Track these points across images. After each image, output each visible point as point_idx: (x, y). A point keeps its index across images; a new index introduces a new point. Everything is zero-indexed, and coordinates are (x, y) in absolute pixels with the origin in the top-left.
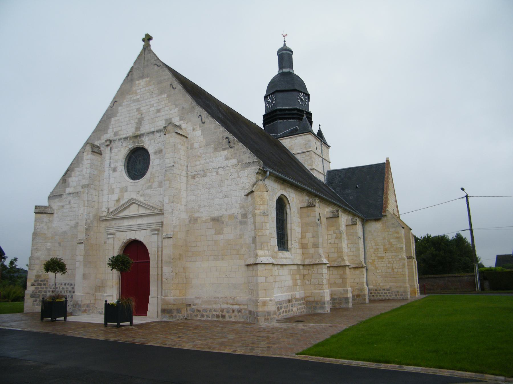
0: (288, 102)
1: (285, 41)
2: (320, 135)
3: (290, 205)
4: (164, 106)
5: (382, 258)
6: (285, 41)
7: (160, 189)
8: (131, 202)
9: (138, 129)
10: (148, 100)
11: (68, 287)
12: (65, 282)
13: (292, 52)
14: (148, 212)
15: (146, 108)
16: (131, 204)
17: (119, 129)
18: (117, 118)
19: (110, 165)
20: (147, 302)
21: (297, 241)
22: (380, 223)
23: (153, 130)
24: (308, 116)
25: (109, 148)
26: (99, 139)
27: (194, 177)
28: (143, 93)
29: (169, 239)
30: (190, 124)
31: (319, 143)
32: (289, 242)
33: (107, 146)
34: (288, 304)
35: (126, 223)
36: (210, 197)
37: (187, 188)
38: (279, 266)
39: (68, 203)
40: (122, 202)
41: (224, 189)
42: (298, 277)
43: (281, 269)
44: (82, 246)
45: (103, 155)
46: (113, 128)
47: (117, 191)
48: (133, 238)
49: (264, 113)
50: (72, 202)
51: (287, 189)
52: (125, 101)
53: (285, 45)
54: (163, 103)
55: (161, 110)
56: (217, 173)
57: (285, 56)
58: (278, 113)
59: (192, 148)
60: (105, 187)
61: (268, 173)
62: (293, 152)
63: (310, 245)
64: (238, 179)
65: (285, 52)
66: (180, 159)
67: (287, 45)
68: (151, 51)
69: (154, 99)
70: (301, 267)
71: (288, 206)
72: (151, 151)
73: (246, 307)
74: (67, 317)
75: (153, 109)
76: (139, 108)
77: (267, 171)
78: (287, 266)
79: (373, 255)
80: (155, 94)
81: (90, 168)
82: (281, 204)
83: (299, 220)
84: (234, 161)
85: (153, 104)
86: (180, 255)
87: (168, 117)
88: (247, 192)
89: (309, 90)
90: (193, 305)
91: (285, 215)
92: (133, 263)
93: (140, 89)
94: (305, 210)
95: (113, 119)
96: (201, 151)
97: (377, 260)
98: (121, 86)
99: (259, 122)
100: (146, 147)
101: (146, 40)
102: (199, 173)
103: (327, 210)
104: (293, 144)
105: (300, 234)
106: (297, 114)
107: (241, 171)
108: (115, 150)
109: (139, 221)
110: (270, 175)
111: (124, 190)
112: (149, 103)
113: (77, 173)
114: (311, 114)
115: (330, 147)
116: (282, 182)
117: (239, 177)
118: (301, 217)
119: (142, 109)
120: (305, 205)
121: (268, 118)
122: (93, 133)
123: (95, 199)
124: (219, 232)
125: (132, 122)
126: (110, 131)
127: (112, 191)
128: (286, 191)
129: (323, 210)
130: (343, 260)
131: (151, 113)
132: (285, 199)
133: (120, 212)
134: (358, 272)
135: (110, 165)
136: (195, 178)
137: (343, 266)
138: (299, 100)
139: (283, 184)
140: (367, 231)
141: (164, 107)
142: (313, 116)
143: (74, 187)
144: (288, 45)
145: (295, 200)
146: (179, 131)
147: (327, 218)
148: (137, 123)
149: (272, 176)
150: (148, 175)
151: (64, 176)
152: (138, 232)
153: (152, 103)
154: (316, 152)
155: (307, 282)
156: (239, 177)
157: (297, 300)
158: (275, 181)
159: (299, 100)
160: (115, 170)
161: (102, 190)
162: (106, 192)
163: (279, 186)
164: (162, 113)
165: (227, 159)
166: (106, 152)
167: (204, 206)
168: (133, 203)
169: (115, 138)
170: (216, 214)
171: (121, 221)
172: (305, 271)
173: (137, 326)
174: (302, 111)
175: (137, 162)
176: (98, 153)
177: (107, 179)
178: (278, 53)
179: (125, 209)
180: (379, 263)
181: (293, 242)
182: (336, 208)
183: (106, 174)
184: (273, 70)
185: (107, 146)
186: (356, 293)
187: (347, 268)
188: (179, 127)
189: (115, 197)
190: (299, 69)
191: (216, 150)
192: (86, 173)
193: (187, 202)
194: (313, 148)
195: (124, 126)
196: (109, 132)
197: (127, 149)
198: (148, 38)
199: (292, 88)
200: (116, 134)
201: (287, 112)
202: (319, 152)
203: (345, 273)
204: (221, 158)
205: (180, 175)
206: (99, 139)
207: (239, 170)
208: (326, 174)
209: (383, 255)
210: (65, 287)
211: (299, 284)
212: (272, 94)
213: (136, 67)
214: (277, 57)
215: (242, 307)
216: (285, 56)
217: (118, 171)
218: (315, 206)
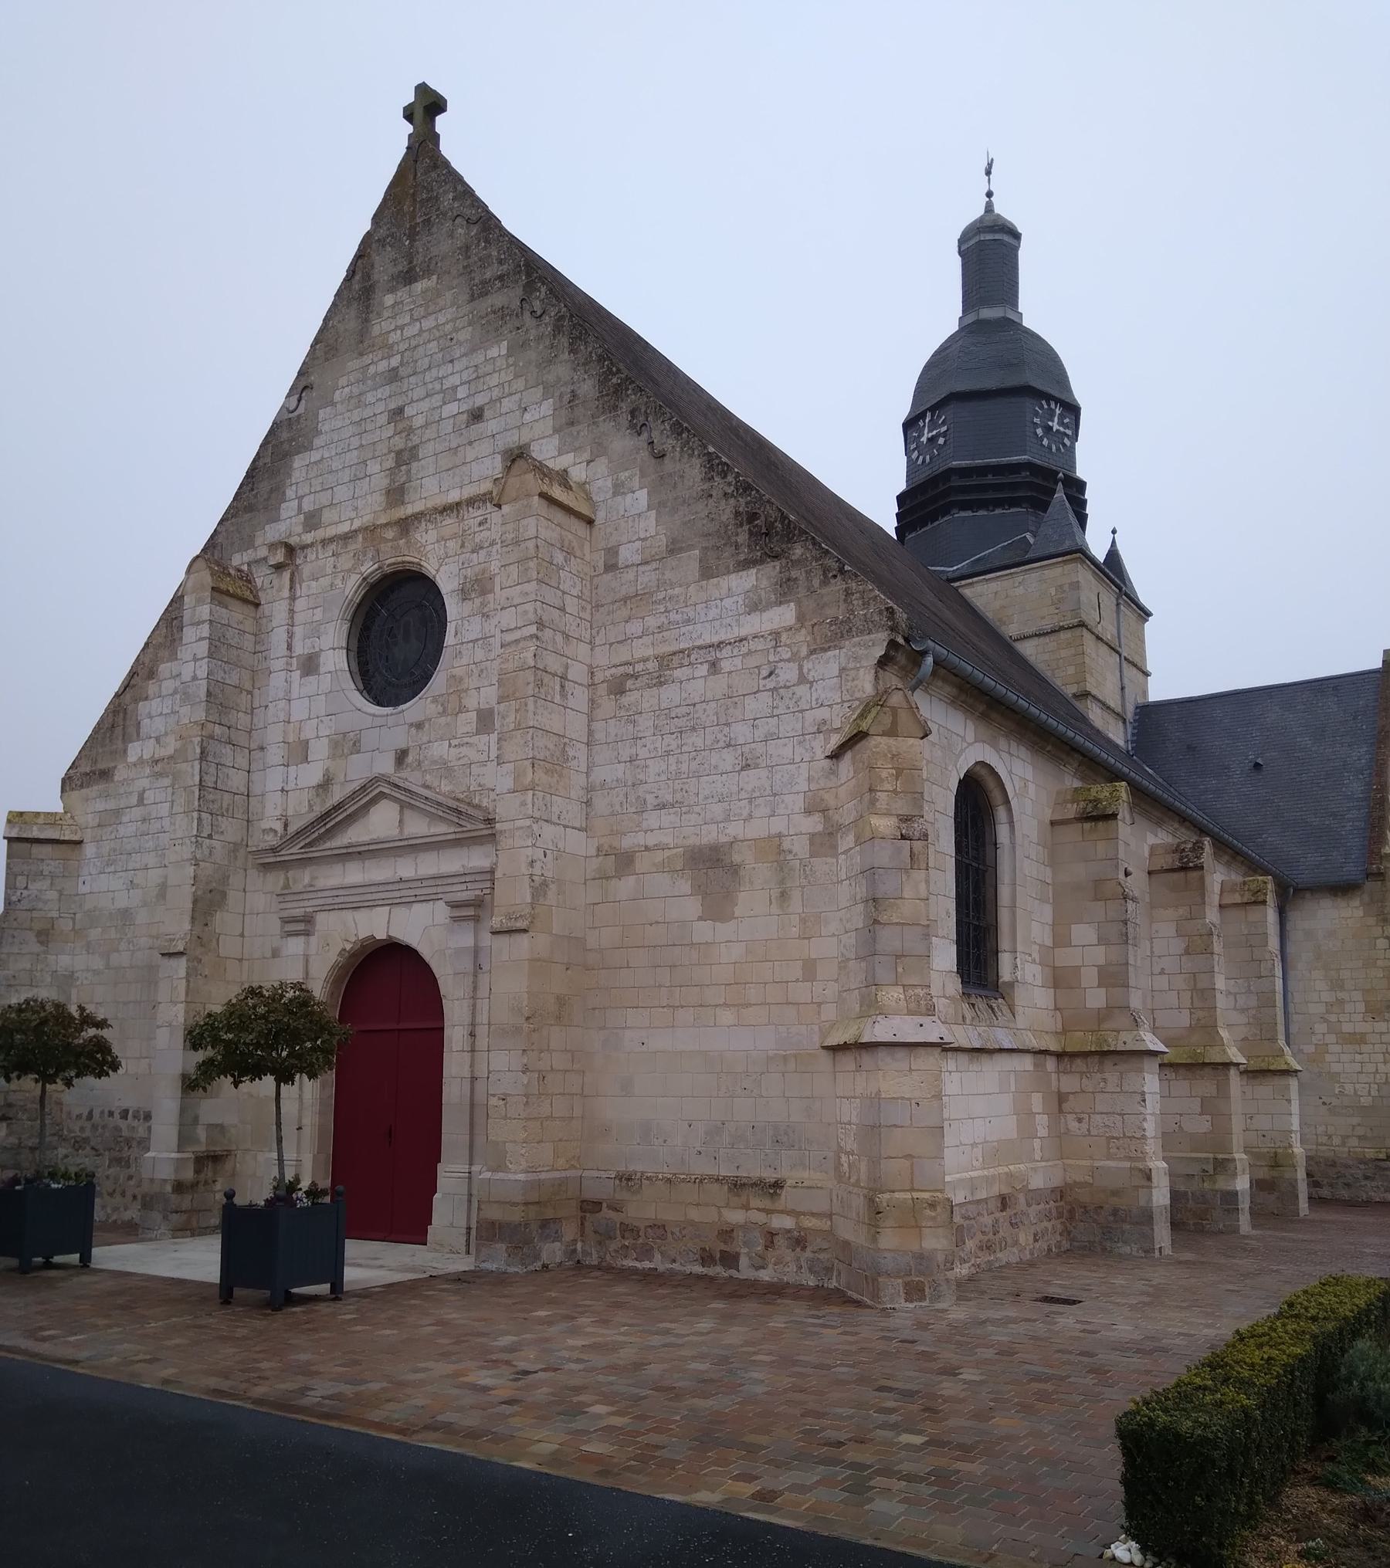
0: (997, 431)
1: (989, 194)
2: (1112, 569)
3: (1010, 810)
4: (496, 393)
5: (1358, 1039)
6: (989, 194)
7: (484, 738)
8: (368, 796)
9: (396, 494)
10: (434, 372)
11: (135, 1123)
12: (125, 1104)
13: (1017, 236)
14: (441, 829)
15: (425, 405)
16: (373, 801)
17: (324, 498)
18: (315, 456)
19: (289, 648)
20: (430, 1186)
21: (1036, 955)
22: (1356, 902)
23: (454, 496)
24: (1073, 492)
25: (287, 575)
26: (250, 544)
27: (618, 688)
28: (414, 343)
29: (518, 937)
30: (601, 466)
31: (1108, 599)
32: (1005, 959)
33: (279, 567)
34: (998, 1215)
35: (354, 874)
36: (684, 767)
37: (590, 733)
38: (963, 1058)
39: (134, 800)
40: (337, 795)
41: (741, 732)
42: (1037, 1101)
43: (975, 1067)
44: (181, 966)
45: (265, 608)
46: (300, 498)
47: (320, 750)
48: (381, 935)
49: (902, 486)
50: (150, 796)
51: (1003, 743)
52: (343, 381)
53: (989, 208)
54: (494, 380)
55: (487, 414)
56: (714, 666)
57: (989, 255)
58: (955, 482)
59: (611, 567)
60: (274, 735)
61: (930, 660)
62: (1011, 630)
63: (1090, 977)
64: (802, 690)
65: (989, 237)
66: (562, 609)
67: (998, 209)
68: (442, 165)
69: (458, 366)
70: (1051, 1064)
71: (1001, 814)
72: (447, 584)
73: (824, 1224)
74: (95, 1251)
75: (452, 408)
76: (400, 411)
77: (923, 653)
78: (997, 1057)
79: (1320, 1028)
80: (460, 343)
81: (210, 656)
82: (976, 801)
83: (1047, 874)
84: (784, 615)
85: (455, 388)
86: (561, 1001)
87: (512, 439)
88: (835, 740)
89: (1081, 391)
90: (609, 1207)
91: (989, 849)
92: (376, 1034)
93: (402, 328)
94: (1072, 833)
95: (298, 462)
96: (647, 577)
97: (1337, 1048)
98: (326, 320)
99: (886, 518)
100: (430, 568)
101: (419, 115)
102: (639, 667)
103: (1152, 839)
104: (1011, 600)
105: (1048, 929)
106: (1030, 485)
107: (812, 652)
108: (308, 588)
109: (406, 868)
110: (934, 673)
111: (346, 744)
112: (438, 387)
113: (168, 686)
114: (1081, 486)
115: (1148, 614)
116: (982, 708)
117: (802, 679)
118: (1053, 861)
119: (409, 411)
120: (1072, 811)
121: (915, 505)
122: (221, 523)
123: (237, 781)
124: (718, 907)
125: (374, 467)
126: (289, 509)
127: (300, 752)
128: (998, 751)
129: (1139, 842)
130: (1214, 1039)
131: (447, 427)
132: (991, 784)
133: (330, 833)
134: (1265, 1089)
135: (289, 648)
136: (622, 692)
137: (1215, 1066)
138: (1039, 431)
139: (984, 717)
140: (1296, 935)
141: (499, 399)
142: (1089, 495)
143: (158, 740)
144: (1004, 209)
145: (1030, 789)
146: (557, 493)
147: (1150, 873)
148: (392, 472)
149: (944, 680)
150: (438, 682)
151: (117, 695)
152: (399, 912)
153: (448, 383)
154: (1099, 630)
155: (1073, 1125)
156: (802, 679)
157: (1034, 1196)
158: (954, 702)
159: (1039, 431)
160: (310, 665)
161: (262, 749)
162: (275, 754)
163: (970, 724)
164: (491, 426)
165: (755, 607)
166: (273, 589)
167: (662, 806)
168: (382, 795)
169: (308, 538)
170: (710, 835)
171: (338, 868)
172: (1064, 1078)
173: (365, 1294)
174: (1050, 475)
175: (396, 632)
176: (245, 601)
177: (282, 704)
178: (961, 242)
179: (351, 819)
180: (1344, 1058)
181: (1021, 963)
182: (1187, 837)
183: (277, 680)
184: (938, 312)
185: (279, 567)
186: (1263, 1173)
187: (1233, 1072)
188: (563, 478)
189: (312, 774)
190: (1040, 307)
191: (707, 572)
192: (195, 678)
193: (589, 789)
194: (1090, 616)
195: (339, 491)
196: (284, 514)
197: (354, 580)
198: (427, 107)
199: (1012, 381)
200: (312, 521)
201: (990, 479)
202: (1108, 631)
203: (1223, 1093)
204: (728, 602)
205: (564, 678)
206: (250, 544)
207: (804, 651)
208: (1130, 716)
209: (1366, 1027)
210: (123, 1124)
211: (1042, 1132)
212: (933, 409)
213: (382, 232)
214: (958, 261)
215: (809, 1223)
216: (989, 255)
217: (322, 670)
218: (1114, 816)
